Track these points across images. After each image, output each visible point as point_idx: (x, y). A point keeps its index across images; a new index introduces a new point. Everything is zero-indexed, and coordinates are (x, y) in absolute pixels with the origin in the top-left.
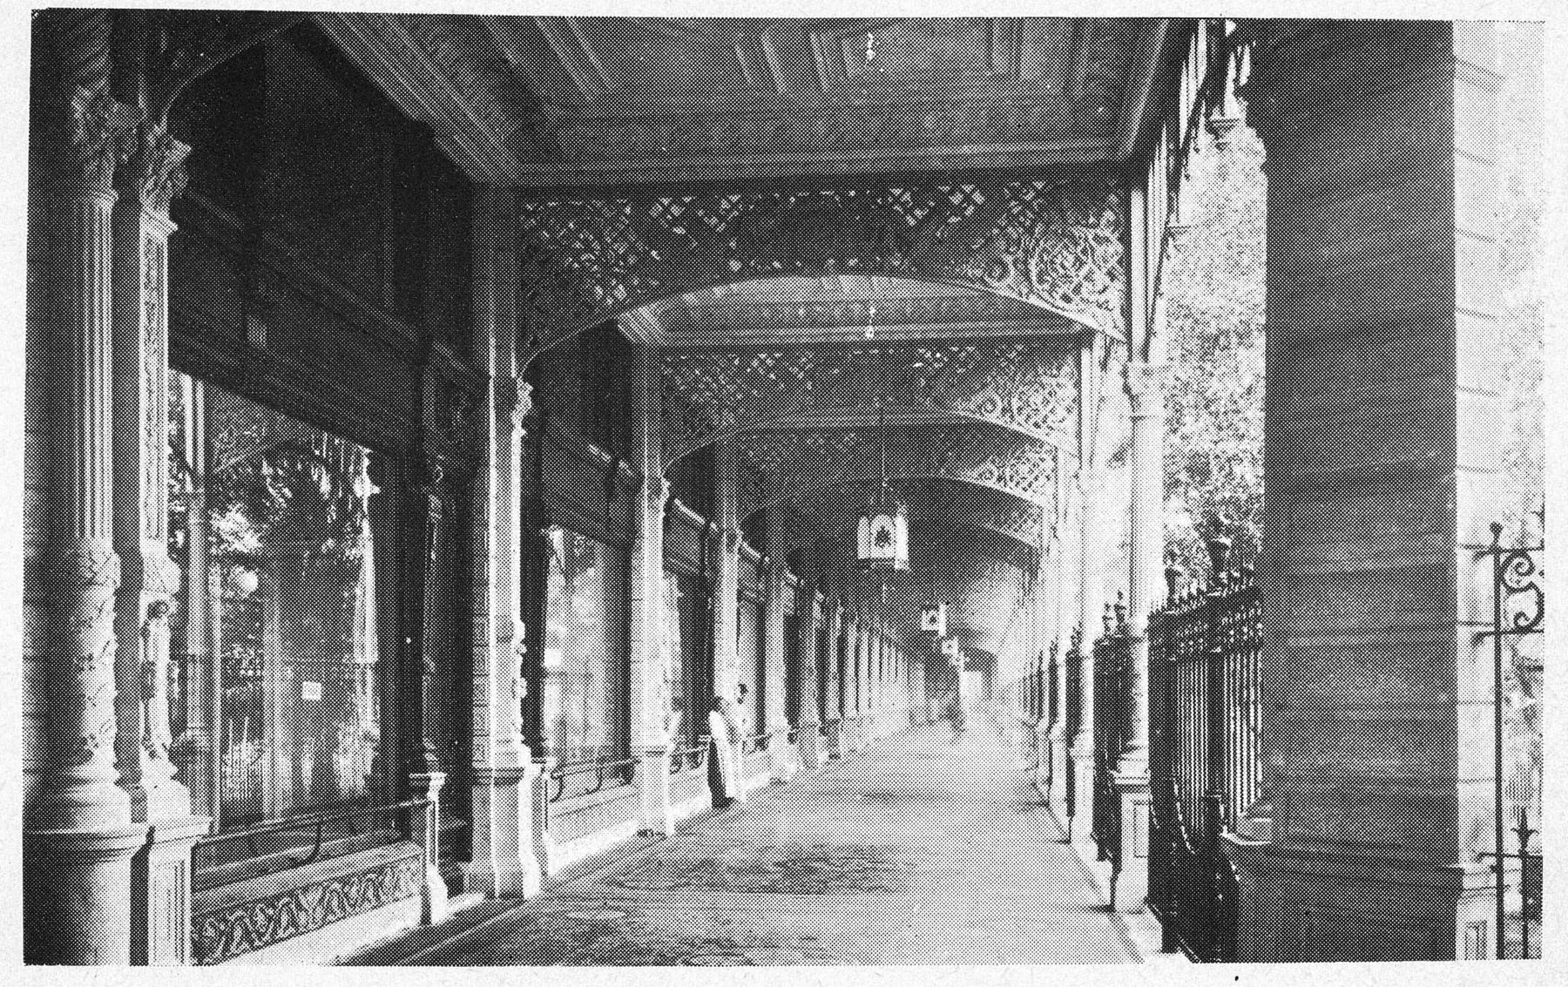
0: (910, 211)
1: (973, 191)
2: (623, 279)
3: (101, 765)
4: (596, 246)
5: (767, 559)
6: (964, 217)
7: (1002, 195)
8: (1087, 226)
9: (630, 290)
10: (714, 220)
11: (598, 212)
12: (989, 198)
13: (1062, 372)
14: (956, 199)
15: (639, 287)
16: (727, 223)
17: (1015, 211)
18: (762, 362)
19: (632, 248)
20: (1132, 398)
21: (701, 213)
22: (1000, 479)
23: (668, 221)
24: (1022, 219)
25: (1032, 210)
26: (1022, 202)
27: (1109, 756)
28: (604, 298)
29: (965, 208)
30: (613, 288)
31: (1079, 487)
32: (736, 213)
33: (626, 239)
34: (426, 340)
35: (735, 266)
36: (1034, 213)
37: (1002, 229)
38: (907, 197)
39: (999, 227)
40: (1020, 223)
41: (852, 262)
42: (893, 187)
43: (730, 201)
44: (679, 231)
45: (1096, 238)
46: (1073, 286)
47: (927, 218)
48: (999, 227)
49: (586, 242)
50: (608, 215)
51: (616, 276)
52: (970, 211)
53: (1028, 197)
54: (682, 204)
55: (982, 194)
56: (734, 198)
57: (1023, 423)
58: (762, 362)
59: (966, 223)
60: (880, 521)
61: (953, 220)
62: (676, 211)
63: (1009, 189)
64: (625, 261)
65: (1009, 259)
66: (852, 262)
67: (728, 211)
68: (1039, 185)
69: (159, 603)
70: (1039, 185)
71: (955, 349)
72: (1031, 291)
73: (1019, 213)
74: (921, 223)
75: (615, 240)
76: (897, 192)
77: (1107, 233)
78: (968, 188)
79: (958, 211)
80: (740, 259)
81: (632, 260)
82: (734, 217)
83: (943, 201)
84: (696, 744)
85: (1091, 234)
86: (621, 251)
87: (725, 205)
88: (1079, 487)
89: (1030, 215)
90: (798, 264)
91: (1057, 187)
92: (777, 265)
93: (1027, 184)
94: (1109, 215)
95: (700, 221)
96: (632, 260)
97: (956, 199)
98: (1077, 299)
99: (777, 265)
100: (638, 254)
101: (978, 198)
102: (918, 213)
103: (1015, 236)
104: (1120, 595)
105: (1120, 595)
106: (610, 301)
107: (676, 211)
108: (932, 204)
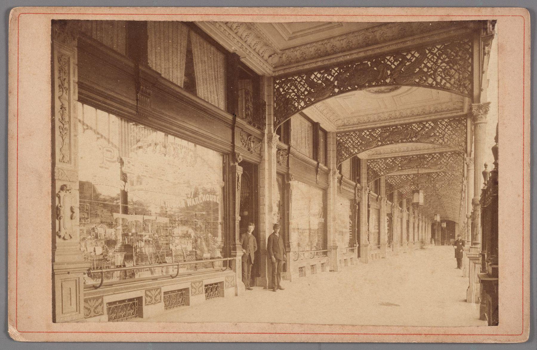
2: (303, 99)
4: (379, 167)
5: (393, 204)
6: (411, 62)
7: (437, 124)
9: (305, 103)
12: (420, 54)
14: (408, 57)
16: (334, 77)
17: (430, 57)
23: (316, 79)
24: (432, 59)
25: (444, 126)
26: (446, 156)
27: (455, 43)
29: (412, 59)
32: (336, 74)
33: (304, 87)
40: (442, 129)
42: (387, 56)
43: (335, 70)
49: (293, 90)
50: (354, 135)
52: (438, 158)
54: (369, 132)
56: (336, 69)
58: (366, 133)
60: (443, 224)
66: (374, 84)
68: (439, 47)
69: (65, 185)
70: (439, 47)
73: (431, 58)
74: (396, 67)
75: (301, 88)
76: (388, 58)
81: (359, 144)
83: (404, 58)
84: (353, 247)
86: (303, 91)
87: (333, 71)
89: (435, 57)
90: (393, 142)
92: (349, 88)
95: (372, 135)
99: (349, 88)
100: (360, 143)
101: (417, 55)
106: (300, 107)
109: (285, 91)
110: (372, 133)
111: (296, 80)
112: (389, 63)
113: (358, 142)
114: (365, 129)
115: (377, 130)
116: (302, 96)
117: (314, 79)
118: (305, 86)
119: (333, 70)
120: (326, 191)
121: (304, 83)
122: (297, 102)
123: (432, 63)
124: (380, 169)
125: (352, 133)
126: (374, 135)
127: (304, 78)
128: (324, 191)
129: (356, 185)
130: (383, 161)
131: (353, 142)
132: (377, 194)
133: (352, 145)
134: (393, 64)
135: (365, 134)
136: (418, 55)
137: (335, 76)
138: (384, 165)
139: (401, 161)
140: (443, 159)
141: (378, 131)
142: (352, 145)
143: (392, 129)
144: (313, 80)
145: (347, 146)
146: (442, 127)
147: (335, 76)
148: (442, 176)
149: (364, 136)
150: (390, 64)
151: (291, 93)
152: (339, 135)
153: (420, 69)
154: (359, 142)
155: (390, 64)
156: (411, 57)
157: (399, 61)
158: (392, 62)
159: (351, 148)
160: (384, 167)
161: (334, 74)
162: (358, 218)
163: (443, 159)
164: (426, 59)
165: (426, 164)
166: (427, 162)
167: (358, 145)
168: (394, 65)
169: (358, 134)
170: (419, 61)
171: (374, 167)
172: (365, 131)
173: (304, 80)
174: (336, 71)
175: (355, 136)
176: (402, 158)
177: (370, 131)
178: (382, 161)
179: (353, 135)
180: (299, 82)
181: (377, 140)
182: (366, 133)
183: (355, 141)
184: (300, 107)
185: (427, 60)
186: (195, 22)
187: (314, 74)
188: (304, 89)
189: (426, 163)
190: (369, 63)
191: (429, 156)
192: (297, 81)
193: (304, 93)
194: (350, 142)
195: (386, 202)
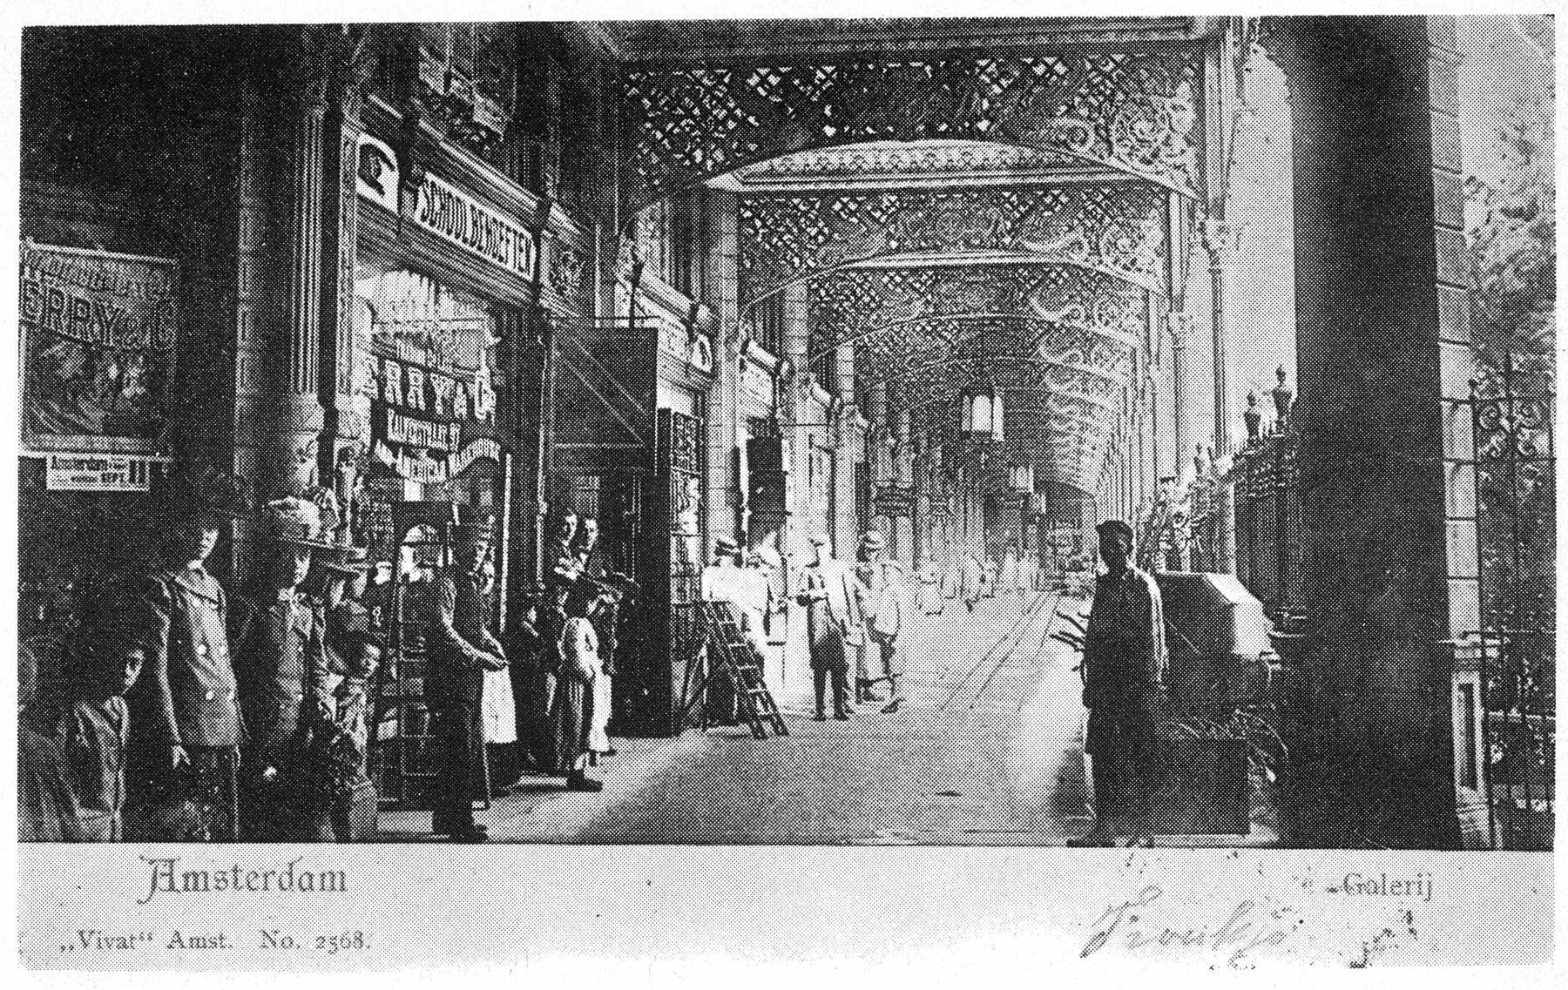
8: (1164, 95)
11: (796, 207)
13: (1179, 91)
15: (738, 150)
18: (845, 205)
19: (731, 115)
20: (1212, 253)
21: (796, 82)
22: (1088, 317)
26: (1101, 73)
28: (704, 161)
30: (712, 152)
31: (1205, 244)
32: (893, 209)
34: (544, 208)
35: (830, 131)
36: (1112, 82)
37: (1084, 97)
38: (1014, 198)
39: (1080, 95)
41: (943, 127)
43: (824, 72)
45: (1174, 107)
46: (1151, 150)
48: (1080, 95)
51: (716, 140)
53: (1099, 199)
54: (778, 74)
56: (829, 69)
57: (1110, 265)
58: (845, 205)
63: (1090, 61)
64: (725, 127)
65: (1085, 242)
67: (823, 82)
71: (1029, 60)
76: (983, 63)
77: (1183, 102)
78: (1050, 60)
79: (1049, 208)
81: (821, 239)
85: (1168, 102)
87: (820, 75)
88: (1205, 244)
91: (1136, 60)
92: (870, 131)
93: (1107, 56)
94: (1184, 88)
97: (1040, 70)
103: (1096, 104)
104: (1281, 375)
105: (1281, 375)
106: (710, 163)
107: (774, 80)
109: (768, 227)
111: (796, 207)
112: (983, 77)
113: (726, 118)
114: (844, 193)
115: (818, 72)
116: (719, 132)
117: (757, 85)
119: (818, 72)
120: (704, 397)
121: (726, 94)
122: (704, 149)
124: (857, 309)
125: (796, 201)
127: (726, 80)
128: (696, 397)
129: (694, 309)
130: (817, 206)
131: (801, 230)
132: (688, 293)
133: (853, 306)
134: (996, 81)
135: (842, 210)
138: (821, 224)
139: (932, 285)
140: (1081, 216)
141: (823, 77)
142: (853, 306)
145: (676, 130)
146: (1103, 82)
148: (1061, 282)
149: (838, 214)
150: (988, 81)
151: (783, 234)
152: (748, 203)
154: (873, 299)
155: (988, 81)
156: (1045, 73)
159: (792, 250)
162: (1473, 745)
167: (730, 133)
168: (1000, 86)
169: (726, 80)
171: (834, 301)
172: (845, 200)
173: (726, 85)
175: (808, 212)
176: (961, 325)
177: (783, 70)
179: (802, 207)
181: (885, 231)
182: (763, 81)
183: (809, 230)
184: (710, 163)
186: (570, 25)
187: (758, 74)
188: (816, 230)
190: (928, 68)
191: (1029, 272)
192: (799, 210)
194: (789, 231)
195: (743, 352)
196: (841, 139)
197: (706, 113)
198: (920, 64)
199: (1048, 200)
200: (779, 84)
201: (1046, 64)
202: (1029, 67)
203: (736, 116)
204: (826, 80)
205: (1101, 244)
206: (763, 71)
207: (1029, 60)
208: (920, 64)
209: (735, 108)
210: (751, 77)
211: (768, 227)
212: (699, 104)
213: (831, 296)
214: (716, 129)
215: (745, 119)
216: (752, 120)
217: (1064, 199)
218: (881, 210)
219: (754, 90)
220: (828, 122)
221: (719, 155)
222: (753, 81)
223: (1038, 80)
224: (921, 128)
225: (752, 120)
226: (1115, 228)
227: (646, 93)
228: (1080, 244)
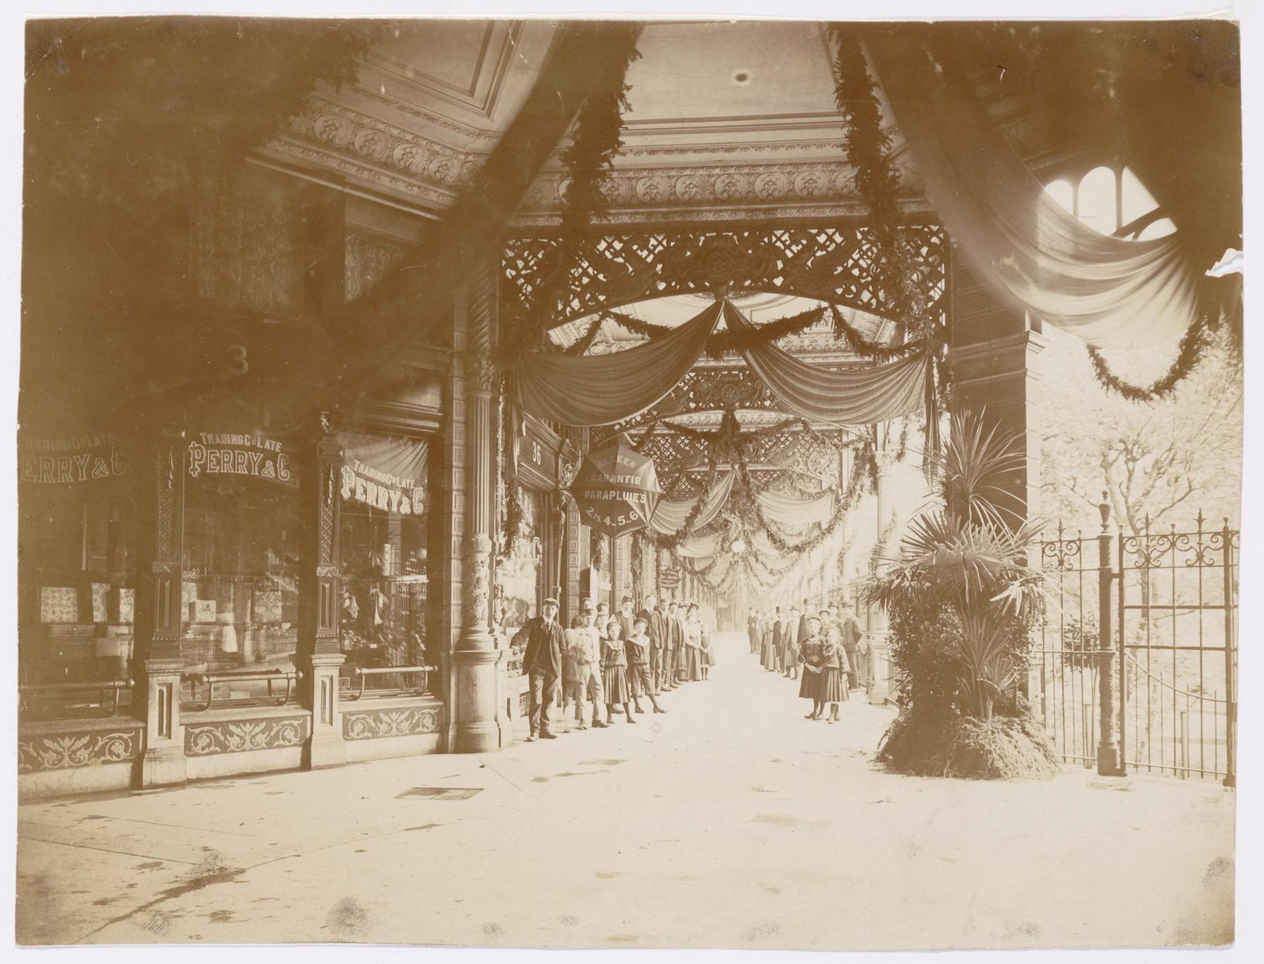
0: (789, 247)
1: (834, 233)
3: (482, 626)
9: (582, 302)
10: (645, 253)
17: (864, 248)
21: (635, 247)
28: (564, 309)
29: (829, 246)
32: (660, 248)
38: (786, 237)
41: (748, 404)
43: (657, 240)
44: (688, 448)
47: (773, 446)
55: (841, 235)
59: (786, 448)
61: (782, 446)
62: (687, 441)
65: (800, 460)
66: (748, 404)
67: (655, 247)
72: (808, 470)
76: (779, 233)
79: (783, 443)
80: (695, 403)
82: (660, 252)
83: (812, 240)
86: (577, 275)
87: (653, 242)
96: (671, 458)
97: (822, 239)
98: (824, 473)
99: (712, 405)
101: (838, 239)
102: (794, 248)
107: (687, 441)
108: (804, 242)
110: (635, 247)
111: (659, 442)
112: (779, 244)
116: (575, 286)
117: (605, 250)
118: (583, 264)
123: (869, 262)
125: (659, 439)
126: (639, 252)
136: (842, 239)
137: (656, 252)
140: (799, 447)
141: (656, 243)
143: (702, 238)
144: (602, 253)
146: (868, 249)
147: (656, 252)
150: (783, 248)
153: (846, 269)
154: (686, 487)
157: (802, 244)
158: (787, 243)
160: (671, 454)
161: (655, 247)
163: (799, 447)
164: (858, 250)
165: (769, 398)
166: (766, 451)
168: (792, 251)
170: (842, 254)
174: (660, 243)
178: (667, 441)
180: (663, 445)
182: (610, 246)
185: (859, 252)
189: (763, 452)
190: (741, 374)
193: (668, 457)
196: (697, 410)
197: (662, 453)
198: (737, 372)
199: (783, 439)
200: (622, 250)
201: (827, 234)
202: (779, 438)
203: (588, 273)
204: (658, 246)
205: (808, 462)
206: (683, 438)
207: (814, 231)
208: (737, 372)
209: (588, 268)
210: (599, 243)
211: (531, 268)
212: (659, 450)
213: (531, 268)
214: (573, 284)
215: (595, 276)
216: (601, 277)
217: (790, 439)
218: (648, 250)
219: (602, 253)
220: (692, 400)
221: (576, 304)
222: (679, 441)
223: (823, 247)
224: (738, 404)
225: (601, 277)
226: (815, 453)
227: (520, 257)
228: (798, 462)
